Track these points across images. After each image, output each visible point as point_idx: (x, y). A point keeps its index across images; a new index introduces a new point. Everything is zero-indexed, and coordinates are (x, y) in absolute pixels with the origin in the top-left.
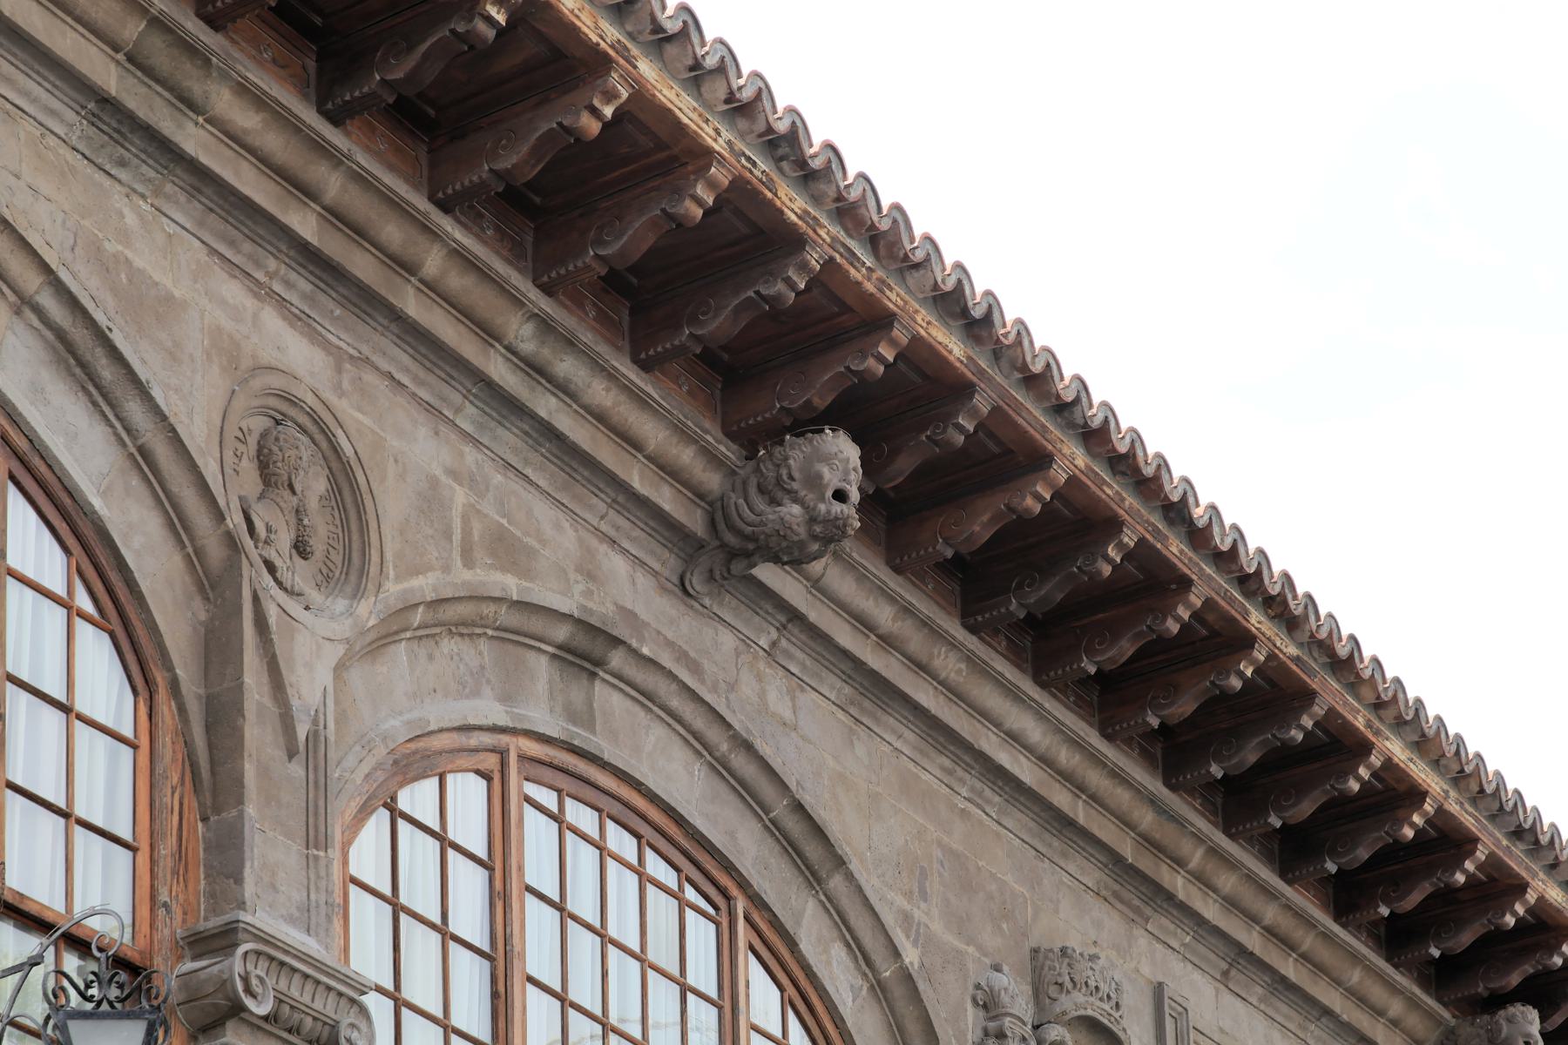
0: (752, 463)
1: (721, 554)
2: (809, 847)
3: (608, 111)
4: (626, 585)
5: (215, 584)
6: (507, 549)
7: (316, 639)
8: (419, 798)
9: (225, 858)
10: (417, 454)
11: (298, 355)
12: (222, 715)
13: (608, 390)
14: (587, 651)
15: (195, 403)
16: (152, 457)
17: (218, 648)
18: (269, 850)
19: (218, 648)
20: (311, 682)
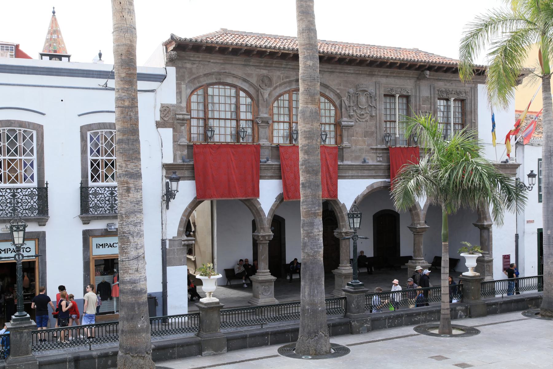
5: (257, 91)
6: (287, 77)
15: (254, 80)
16: (251, 85)
20: (266, 96)
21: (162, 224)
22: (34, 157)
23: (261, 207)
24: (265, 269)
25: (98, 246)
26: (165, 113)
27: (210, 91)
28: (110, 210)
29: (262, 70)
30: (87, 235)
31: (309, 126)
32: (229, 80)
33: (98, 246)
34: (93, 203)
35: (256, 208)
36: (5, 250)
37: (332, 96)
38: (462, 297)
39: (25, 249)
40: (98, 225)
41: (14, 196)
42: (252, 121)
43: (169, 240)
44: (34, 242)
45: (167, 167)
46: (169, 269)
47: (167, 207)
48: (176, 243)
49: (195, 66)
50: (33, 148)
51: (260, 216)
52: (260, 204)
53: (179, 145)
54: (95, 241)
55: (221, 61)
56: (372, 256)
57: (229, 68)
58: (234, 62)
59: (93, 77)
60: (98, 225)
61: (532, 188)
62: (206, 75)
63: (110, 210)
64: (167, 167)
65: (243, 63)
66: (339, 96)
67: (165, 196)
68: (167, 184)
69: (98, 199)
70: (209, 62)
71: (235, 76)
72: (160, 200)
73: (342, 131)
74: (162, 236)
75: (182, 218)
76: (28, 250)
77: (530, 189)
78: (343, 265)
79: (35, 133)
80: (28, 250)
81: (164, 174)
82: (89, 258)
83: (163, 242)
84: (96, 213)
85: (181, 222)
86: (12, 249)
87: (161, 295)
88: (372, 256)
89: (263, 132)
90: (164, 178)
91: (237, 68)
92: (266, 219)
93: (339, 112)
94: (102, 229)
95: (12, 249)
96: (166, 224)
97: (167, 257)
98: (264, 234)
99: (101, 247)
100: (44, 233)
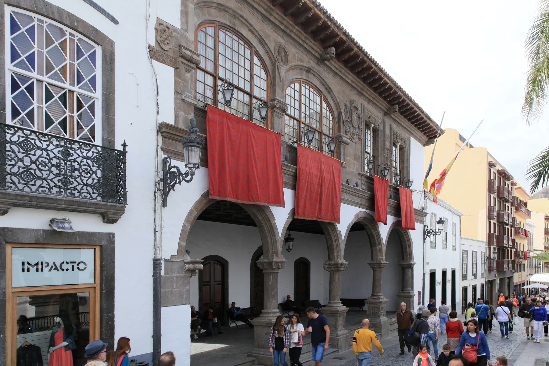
2: (329, 90)
4: (312, 64)
5: (274, 64)
6: (301, 60)
7: (283, 69)
8: (292, 86)
10: (293, 51)
11: (281, 41)
12: (274, 78)
14: (308, 70)
15: (272, 46)
17: (274, 71)
18: (278, 91)
19: (274, 71)
20: (283, 74)
21: (155, 232)
22: (98, 95)
23: (275, 223)
24: (275, 308)
25: (26, 267)
26: (164, 36)
28: (60, 187)
29: (279, 37)
32: (245, 32)
34: (20, 164)
35: (271, 223)
36: (37, 264)
39: (75, 265)
43: (166, 261)
45: (164, 130)
46: (165, 311)
47: (164, 204)
48: (176, 266)
50: (95, 76)
51: (275, 235)
52: (274, 219)
53: (183, 100)
56: (248, 306)
61: (193, 175)
63: (60, 187)
64: (164, 130)
67: (161, 183)
68: (164, 162)
69: (34, 158)
71: (252, 30)
72: (152, 188)
74: (155, 254)
75: (184, 226)
77: (189, 178)
78: (336, 301)
79: (99, 50)
81: (160, 144)
82: (4, 293)
83: (156, 263)
84: (27, 189)
85: (183, 231)
86: (51, 264)
87: (151, 358)
88: (248, 306)
89: (277, 122)
90: (160, 151)
92: (280, 240)
93: (336, 125)
94: (37, 230)
95: (51, 264)
96: (161, 233)
97: (162, 290)
98: (278, 261)
100: (111, 237)
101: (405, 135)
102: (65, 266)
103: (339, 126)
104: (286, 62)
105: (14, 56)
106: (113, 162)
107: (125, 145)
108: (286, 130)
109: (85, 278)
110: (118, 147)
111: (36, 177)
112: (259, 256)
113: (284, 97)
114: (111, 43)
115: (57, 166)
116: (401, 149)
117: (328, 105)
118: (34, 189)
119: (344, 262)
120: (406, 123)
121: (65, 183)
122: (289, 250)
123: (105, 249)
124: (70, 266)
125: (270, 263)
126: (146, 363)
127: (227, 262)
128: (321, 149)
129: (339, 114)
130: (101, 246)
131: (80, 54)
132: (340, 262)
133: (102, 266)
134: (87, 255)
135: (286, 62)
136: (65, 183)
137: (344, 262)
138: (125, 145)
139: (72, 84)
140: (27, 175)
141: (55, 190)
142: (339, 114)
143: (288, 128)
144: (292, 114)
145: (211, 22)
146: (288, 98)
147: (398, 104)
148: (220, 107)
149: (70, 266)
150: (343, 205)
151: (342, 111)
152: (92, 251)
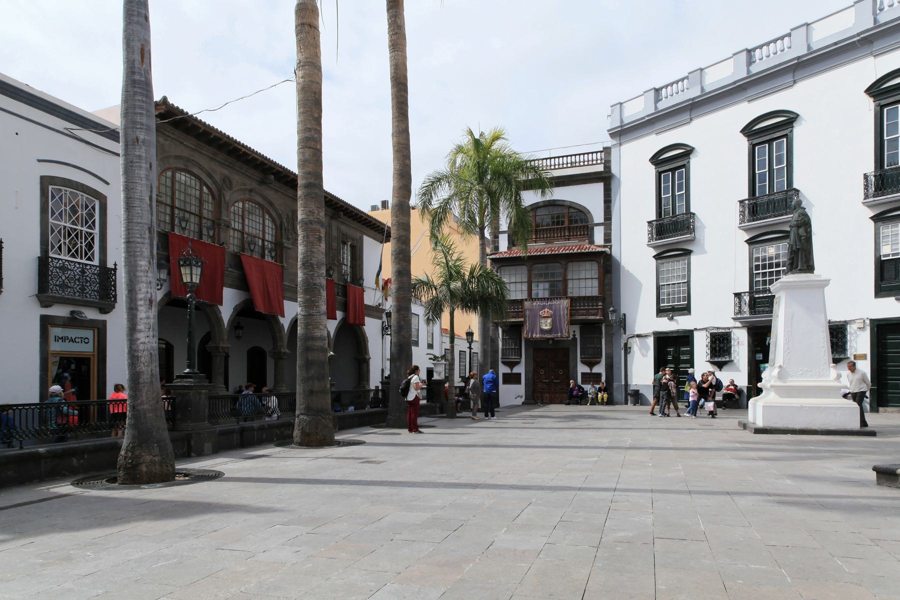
0: (844, 365)
1: (262, 182)
2: (271, 204)
3: (116, 411)
4: (254, 185)
5: (220, 191)
6: (244, 184)
7: (228, 195)
8: (236, 204)
9: (220, 212)
10: (236, 178)
11: (226, 172)
12: (220, 201)
13: (671, 319)
14: (251, 191)
15: (218, 178)
16: (215, 182)
17: (220, 196)
18: (224, 212)
19: (220, 196)
20: (227, 198)
22: (96, 231)
25: (57, 339)
27: (178, 175)
30: (46, 323)
31: (698, 378)
32: (196, 170)
33: (57, 339)
37: (274, 214)
38: (661, 384)
40: (60, 311)
41: (83, 272)
42: (213, 222)
44: (92, 332)
49: (167, 143)
54: (55, 331)
55: (211, 155)
57: (197, 158)
58: (204, 152)
59: (58, 116)
60: (60, 311)
62: (177, 157)
65: (211, 155)
66: (279, 215)
70: (182, 143)
71: (200, 167)
73: (282, 252)
76: (86, 341)
80: (86, 341)
91: (204, 159)
99: (60, 341)
101: (357, 235)
102: (77, 340)
103: (281, 234)
104: (231, 188)
105: (53, 213)
106: (106, 275)
107: (115, 265)
108: (231, 241)
109: (87, 348)
110: (110, 265)
111: (68, 287)
112: (207, 342)
113: (228, 216)
114: (105, 197)
115: (79, 280)
116: (352, 247)
117: (271, 216)
118: (61, 294)
119: (287, 351)
120: (355, 224)
121: (83, 289)
122: (238, 337)
123: (100, 329)
124: (79, 340)
125: (217, 348)
126: (465, 141)
127: (173, 347)
128: (263, 256)
129: (281, 222)
130: (98, 329)
131: (87, 207)
132: (283, 350)
133: (98, 341)
134: (89, 334)
135: (231, 188)
136: (83, 289)
137: (287, 351)
138: (115, 265)
139: (82, 226)
140: (64, 286)
141: (77, 294)
142: (281, 222)
143: (232, 243)
144: (237, 227)
145: (169, 169)
146: (232, 215)
147: (342, 211)
148: (177, 232)
149: (79, 340)
150: (285, 301)
151: (284, 220)
152: (92, 332)
